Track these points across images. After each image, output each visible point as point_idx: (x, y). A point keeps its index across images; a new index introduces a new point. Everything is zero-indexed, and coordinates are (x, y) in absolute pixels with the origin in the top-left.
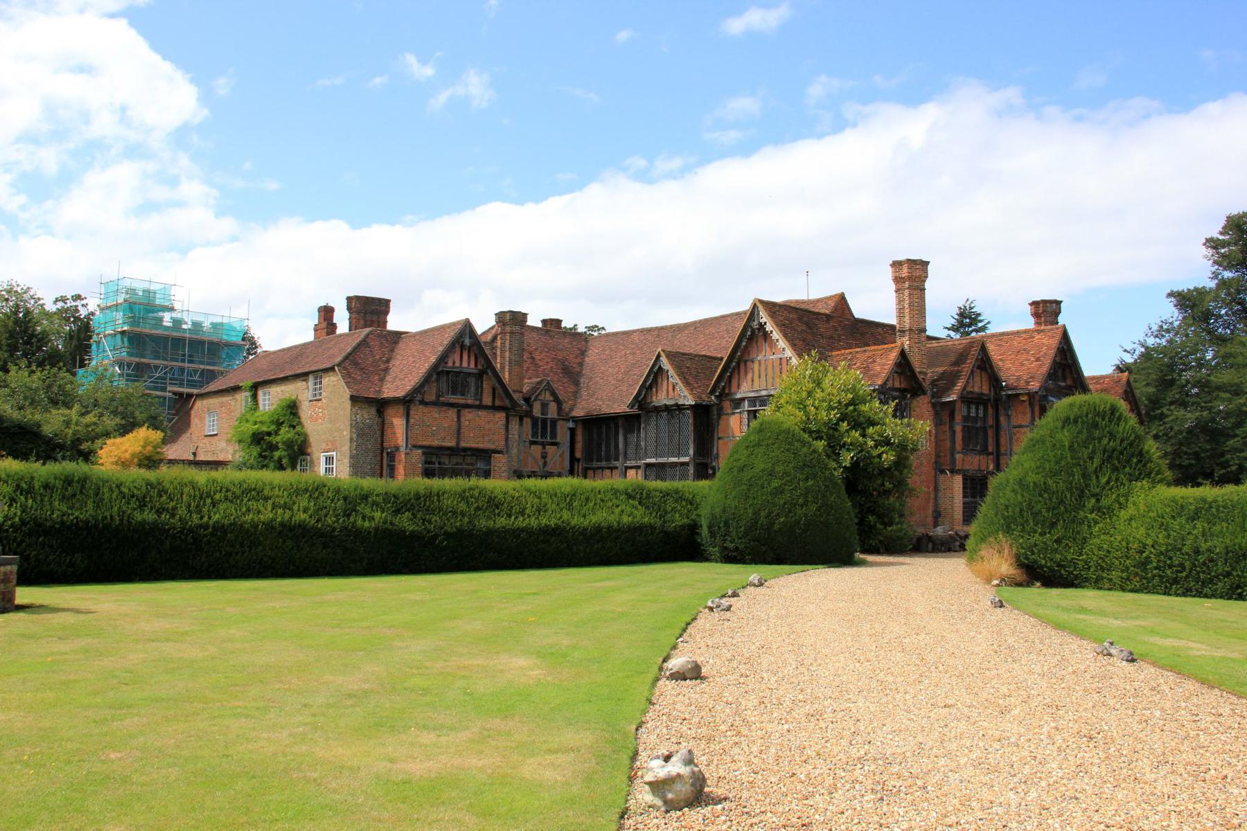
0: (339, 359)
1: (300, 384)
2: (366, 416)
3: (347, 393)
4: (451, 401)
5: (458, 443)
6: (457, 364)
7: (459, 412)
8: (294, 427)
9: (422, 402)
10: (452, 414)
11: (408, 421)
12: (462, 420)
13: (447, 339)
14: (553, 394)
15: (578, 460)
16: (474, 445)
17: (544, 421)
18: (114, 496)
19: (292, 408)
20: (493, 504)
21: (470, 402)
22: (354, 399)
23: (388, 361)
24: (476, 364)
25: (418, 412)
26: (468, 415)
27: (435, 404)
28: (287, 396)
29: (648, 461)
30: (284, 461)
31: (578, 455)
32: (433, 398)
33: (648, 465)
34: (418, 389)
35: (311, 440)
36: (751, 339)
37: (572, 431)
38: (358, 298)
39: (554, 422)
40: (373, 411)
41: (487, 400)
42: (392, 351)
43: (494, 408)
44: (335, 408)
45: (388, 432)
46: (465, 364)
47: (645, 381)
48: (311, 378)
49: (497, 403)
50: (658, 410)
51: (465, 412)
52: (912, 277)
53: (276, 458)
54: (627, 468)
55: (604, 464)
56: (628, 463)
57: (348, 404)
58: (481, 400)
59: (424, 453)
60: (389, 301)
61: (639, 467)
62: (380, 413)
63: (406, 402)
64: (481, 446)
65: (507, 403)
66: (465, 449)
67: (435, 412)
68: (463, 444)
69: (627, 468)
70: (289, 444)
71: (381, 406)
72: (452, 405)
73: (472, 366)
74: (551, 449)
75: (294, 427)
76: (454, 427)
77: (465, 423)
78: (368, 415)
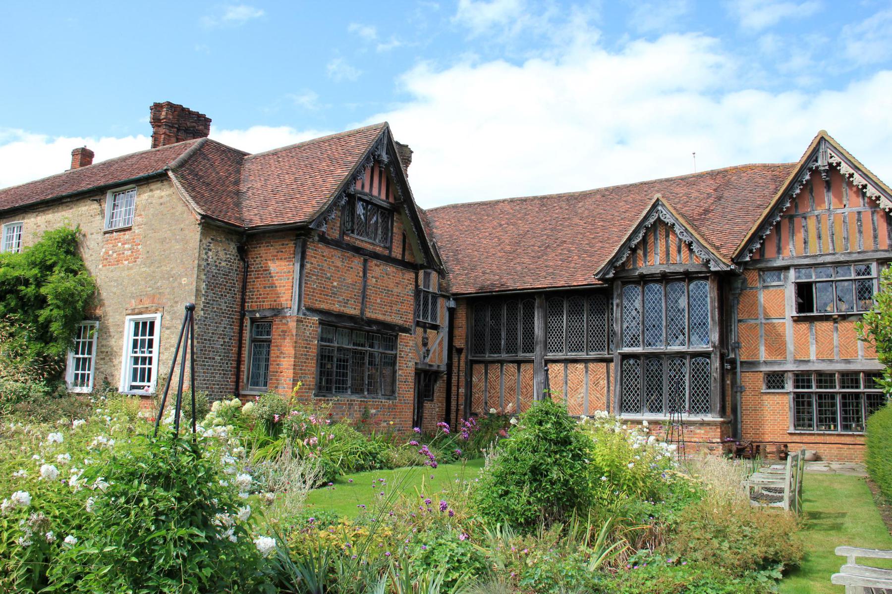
0: (173, 164)
1: (87, 209)
2: (222, 254)
3: (197, 210)
4: (358, 244)
5: (362, 312)
6: (367, 190)
7: (365, 261)
8: (75, 273)
9: (323, 239)
10: (357, 262)
11: (302, 266)
13: (361, 149)
15: (460, 351)
16: (381, 317)
19: (70, 244)
21: (378, 250)
22: (209, 224)
23: (237, 183)
24: (387, 197)
25: (318, 254)
26: (377, 269)
27: (337, 244)
28: (59, 226)
29: (626, 350)
30: (55, 328)
31: (459, 343)
33: (625, 357)
34: (323, 216)
35: (104, 294)
36: (808, 187)
37: (452, 311)
38: (170, 105)
39: (435, 297)
40: (233, 248)
41: (397, 253)
42: (238, 172)
44: (163, 241)
45: (257, 285)
46: (375, 192)
47: (630, 239)
48: (109, 196)
49: (408, 258)
50: (645, 280)
51: (373, 263)
53: (41, 319)
54: (547, 362)
55: (504, 356)
56: (551, 356)
57: (194, 234)
58: (390, 249)
59: (321, 323)
60: (210, 121)
61: (608, 361)
62: (243, 253)
63: (299, 235)
64: (388, 319)
65: (420, 259)
66: (371, 322)
68: (369, 314)
69: (547, 362)
70: (67, 299)
71: (246, 240)
72: (358, 251)
73: (383, 197)
74: (431, 333)
75: (75, 273)
78: (224, 254)
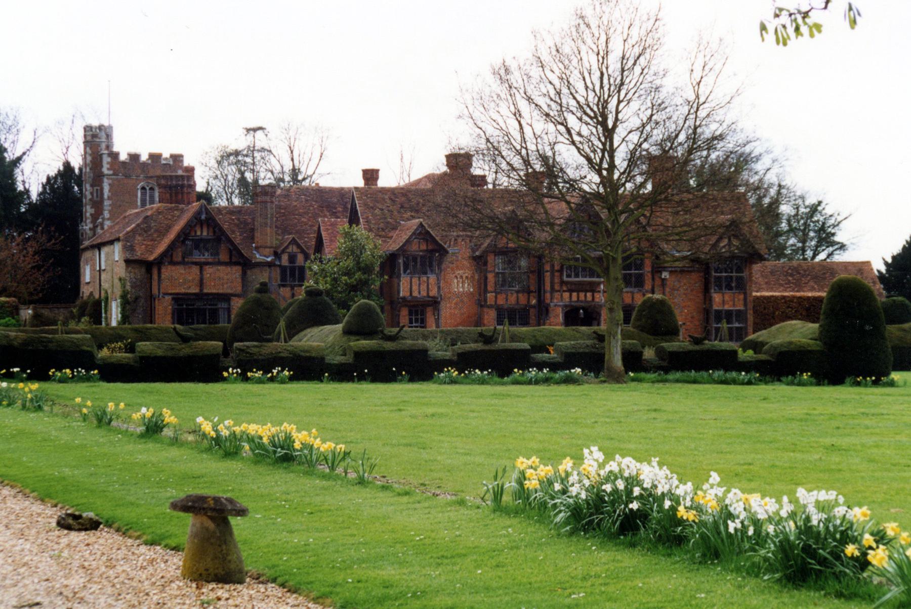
5: (201, 290)
12: (205, 273)
14: (299, 246)
17: (293, 270)
18: (13, 321)
20: (713, 346)
32: (180, 259)
40: (143, 270)
43: (230, 263)
46: (205, 233)
52: (371, 175)
59: (173, 299)
62: (149, 271)
67: (181, 270)
68: (205, 291)
76: (198, 278)
77: (207, 275)
78: (140, 272)
